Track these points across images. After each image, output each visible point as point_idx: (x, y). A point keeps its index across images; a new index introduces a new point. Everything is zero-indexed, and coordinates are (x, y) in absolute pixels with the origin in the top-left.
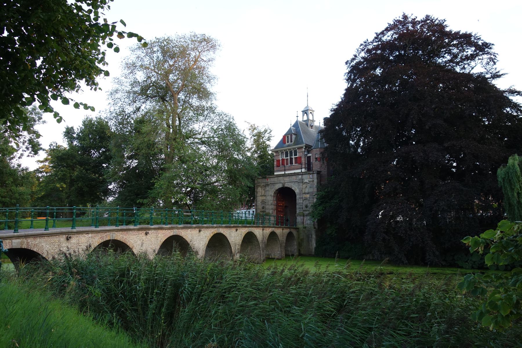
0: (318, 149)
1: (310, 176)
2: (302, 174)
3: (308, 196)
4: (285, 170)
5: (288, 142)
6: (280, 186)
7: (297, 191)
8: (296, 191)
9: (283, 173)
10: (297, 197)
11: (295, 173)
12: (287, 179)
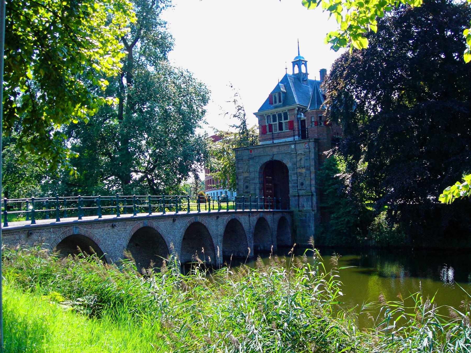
0: (314, 111)
3: (304, 171)
4: (273, 138)
5: (275, 102)
6: (268, 159)
7: (289, 165)
8: (287, 165)
10: (290, 172)
11: (286, 142)
12: (275, 150)
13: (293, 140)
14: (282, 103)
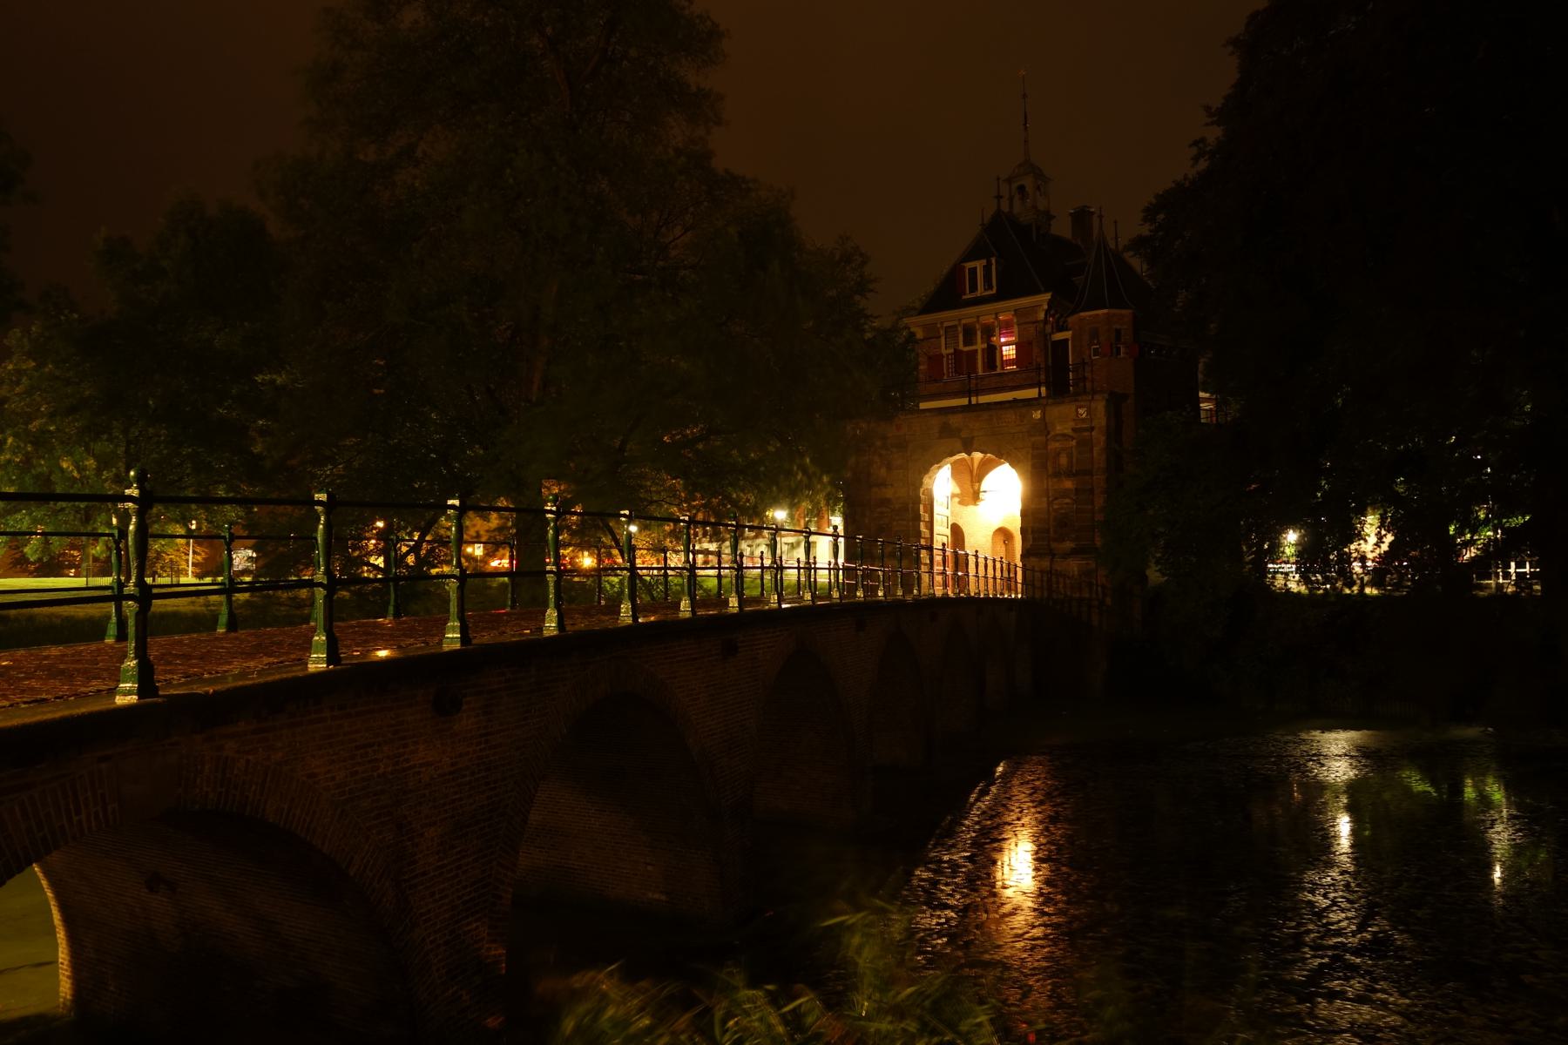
1: (1081, 411)
2: (1028, 403)
5: (974, 288)
9: (964, 401)
13: (967, 403)
14: (994, 291)
